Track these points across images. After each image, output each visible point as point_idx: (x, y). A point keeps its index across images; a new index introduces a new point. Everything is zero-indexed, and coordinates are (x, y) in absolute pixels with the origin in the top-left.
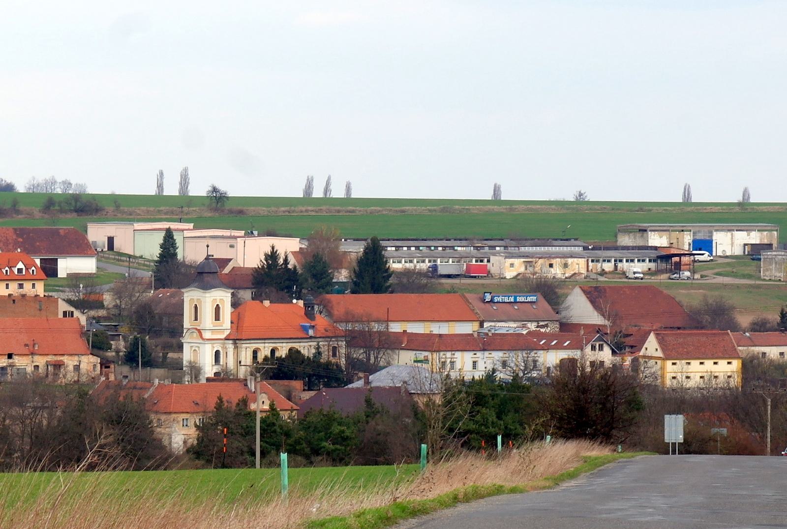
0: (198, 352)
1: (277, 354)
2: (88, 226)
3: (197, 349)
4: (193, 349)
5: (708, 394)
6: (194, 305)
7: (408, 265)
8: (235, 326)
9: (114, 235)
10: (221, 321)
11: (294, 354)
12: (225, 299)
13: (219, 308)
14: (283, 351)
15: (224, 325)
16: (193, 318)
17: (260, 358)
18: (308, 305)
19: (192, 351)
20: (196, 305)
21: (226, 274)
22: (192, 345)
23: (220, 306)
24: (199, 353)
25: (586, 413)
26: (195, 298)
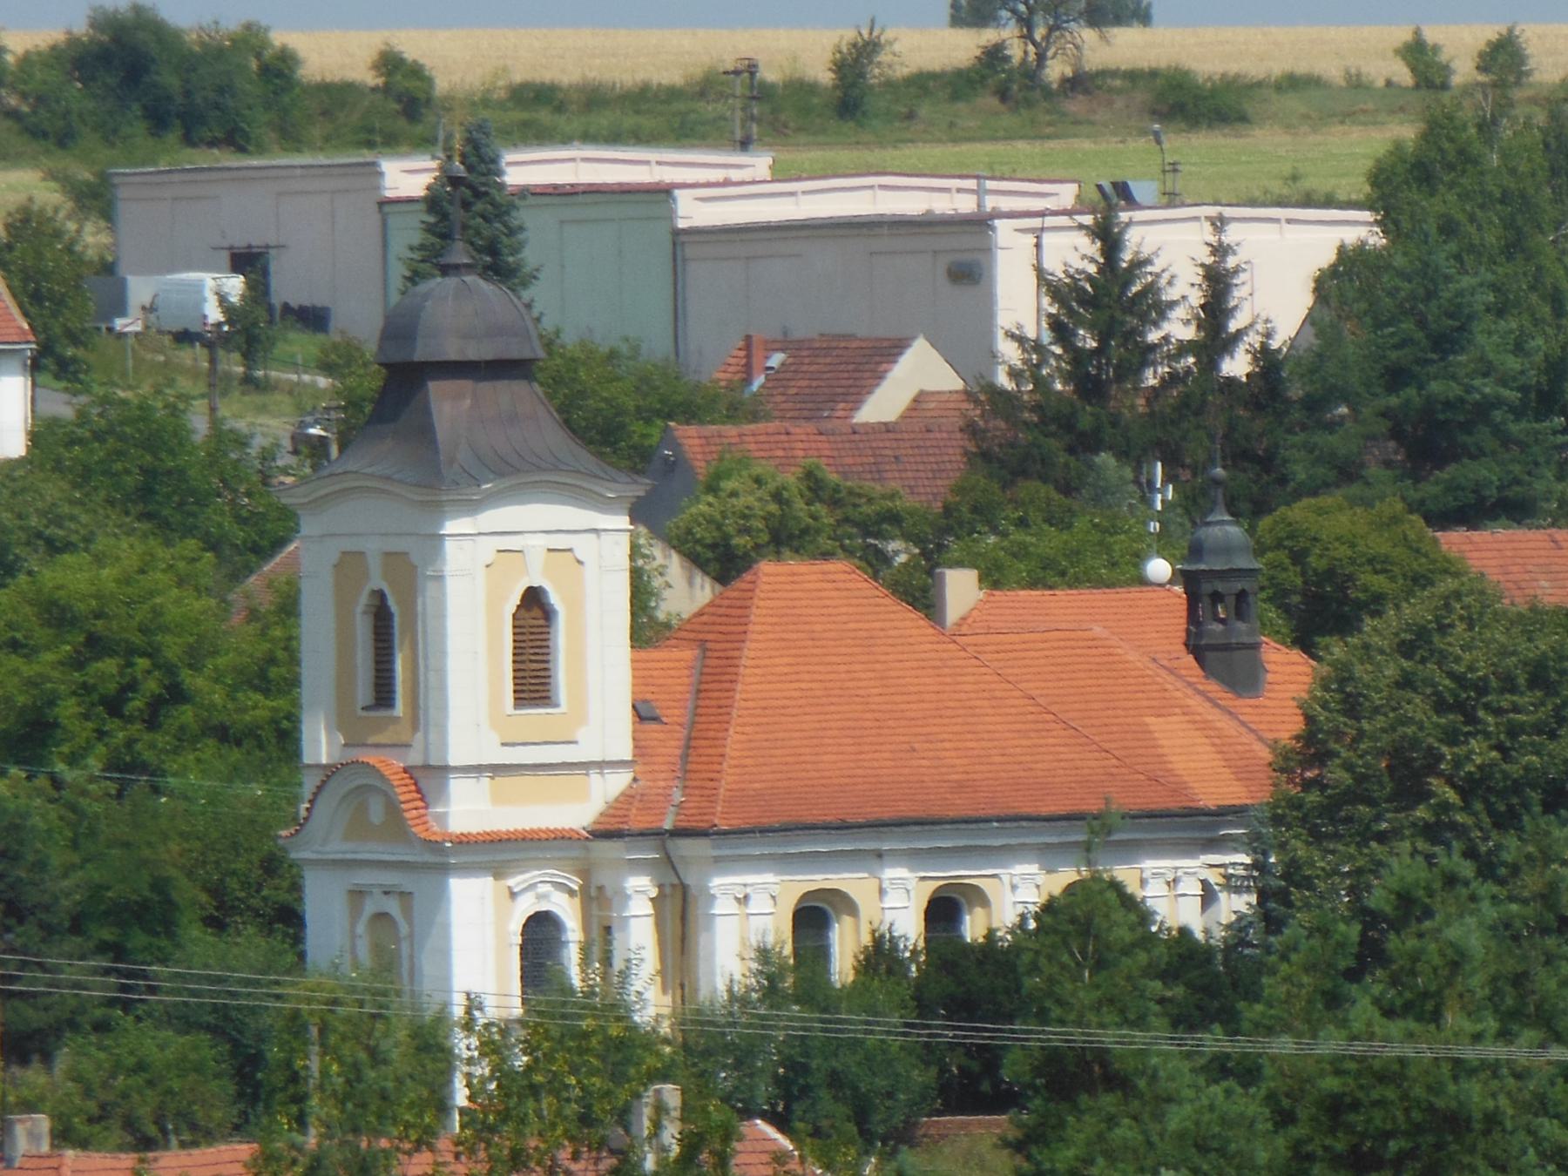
0: (404, 929)
1: (973, 928)
2: (122, 193)
3: (393, 907)
4: (370, 908)
5: (1128, 403)
6: (364, 599)
7: (1397, 1043)
8: (669, 743)
9: (272, 241)
10: (563, 708)
11: (1087, 924)
12: (584, 546)
13: (548, 614)
14: (1014, 893)
15: (581, 734)
16: (364, 691)
17: (844, 949)
18: (1207, 588)
19: (361, 928)
20: (380, 595)
21: (887, 428)
22: (364, 878)
23: (554, 599)
24: (411, 936)
25: (815, 101)
26: (373, 548)
